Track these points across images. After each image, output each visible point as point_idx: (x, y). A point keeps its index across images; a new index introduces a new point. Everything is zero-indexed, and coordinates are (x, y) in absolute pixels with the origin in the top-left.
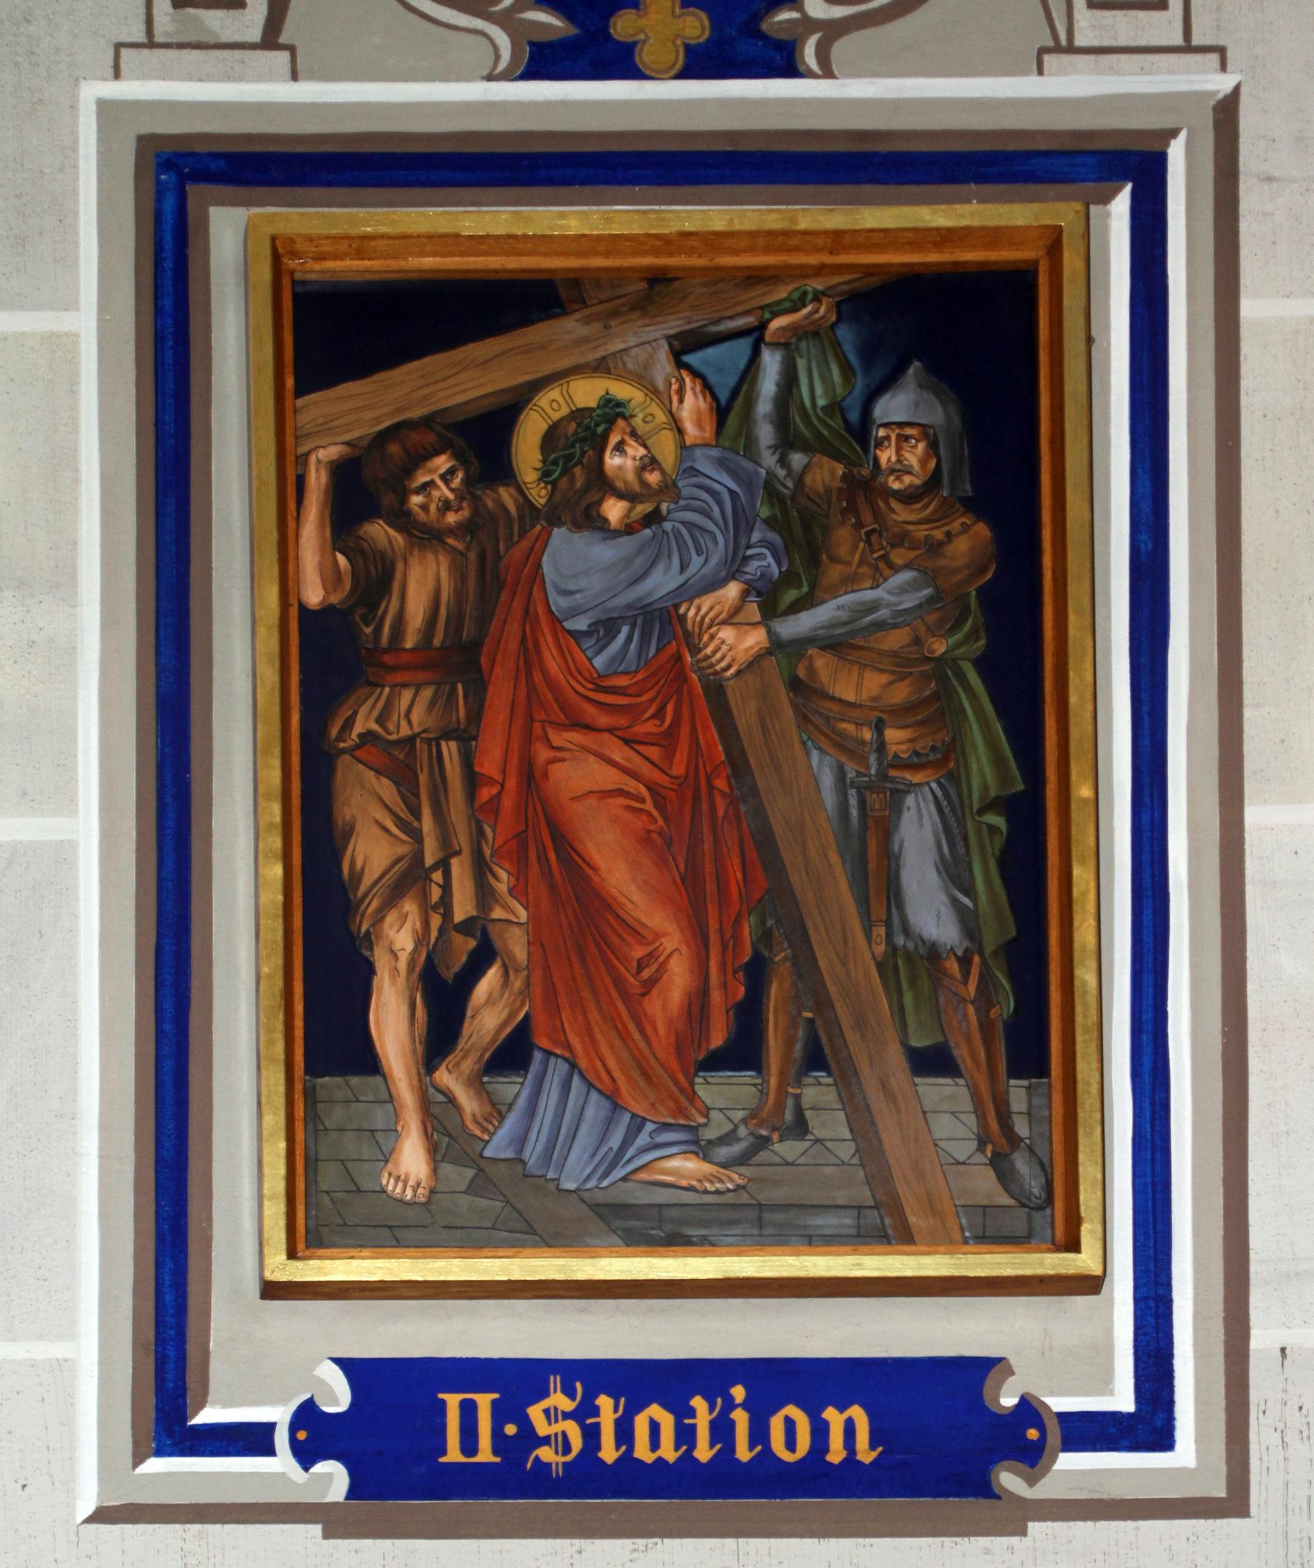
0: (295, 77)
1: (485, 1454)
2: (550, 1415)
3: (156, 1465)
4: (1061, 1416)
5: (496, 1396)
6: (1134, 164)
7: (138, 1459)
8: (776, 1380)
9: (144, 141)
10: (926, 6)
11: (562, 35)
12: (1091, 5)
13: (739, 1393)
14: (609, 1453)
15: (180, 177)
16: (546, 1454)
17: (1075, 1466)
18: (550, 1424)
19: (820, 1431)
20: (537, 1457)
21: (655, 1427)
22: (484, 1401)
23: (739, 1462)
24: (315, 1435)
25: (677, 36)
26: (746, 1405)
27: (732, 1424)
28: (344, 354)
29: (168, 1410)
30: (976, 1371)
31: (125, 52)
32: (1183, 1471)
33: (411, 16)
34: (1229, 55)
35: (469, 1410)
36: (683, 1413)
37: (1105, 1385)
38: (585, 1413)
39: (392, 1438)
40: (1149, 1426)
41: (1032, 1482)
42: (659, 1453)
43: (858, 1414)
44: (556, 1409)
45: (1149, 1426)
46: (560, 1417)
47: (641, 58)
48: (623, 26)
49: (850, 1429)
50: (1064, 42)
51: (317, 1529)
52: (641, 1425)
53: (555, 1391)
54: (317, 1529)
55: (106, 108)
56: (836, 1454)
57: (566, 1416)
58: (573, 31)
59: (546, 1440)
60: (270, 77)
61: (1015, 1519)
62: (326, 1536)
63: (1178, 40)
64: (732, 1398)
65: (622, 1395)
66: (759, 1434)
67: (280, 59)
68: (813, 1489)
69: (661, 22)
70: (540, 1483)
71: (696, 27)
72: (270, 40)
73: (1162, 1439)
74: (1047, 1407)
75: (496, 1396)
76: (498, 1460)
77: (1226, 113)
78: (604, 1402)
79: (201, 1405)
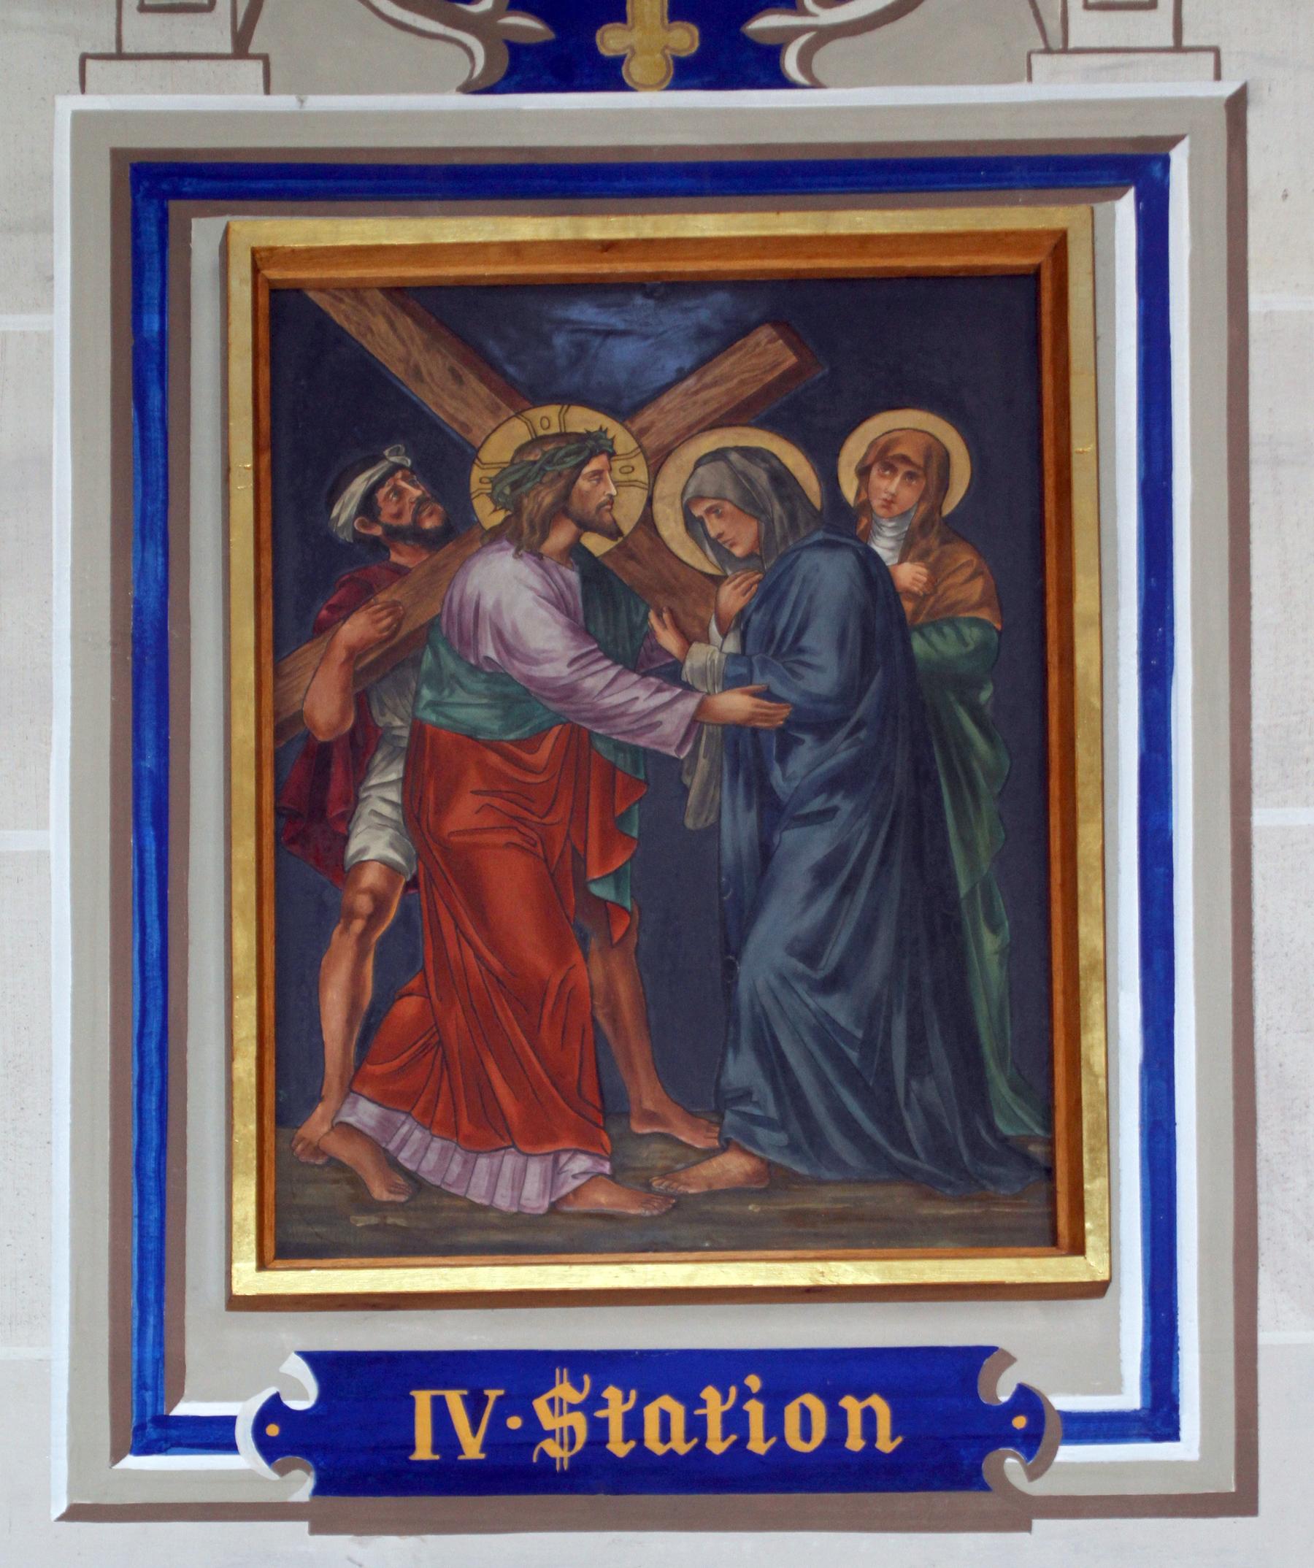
3: (133, 1462)
6: (1135, 168)
7: (117, 1456)
8: (787, 1373)
9: (117, 155)
10: (924, 4)
11: (540, 39)
14: (619, 1447)
15: (157, 191)
16: (552, 1448)
19: (837, 1418)
21: (665, 1418)
24: (282, 1434)
25: (666, 47)
30: (971, 1362)
36: (692, 1401)
37: (1115, 1387)
39: (356, 1438)
41: (1033, 1475)
42: (669, 1446)
44: (561, 1400)
45: (1159, 1418)
46: (565, 1406)
48: (610, 40)
49: (873, 1422)
50: (1056, 43)
51: (304, 1526)
52: (651, 1414)
53: (562, 1382)
54: (304, 1526)
55: (80, 119)
56: (855, 1442)
57: (572, 1408)
58: (551, 35)
59: (551, 1434)
61: (1019, 1515)
65: (632, 1387)
66: (774, 1425)
67: (253, 69)
69: (647, 31)
71: (686, 39)
72: (241, 49)
76: (437, 1457)
77: (1237, 106)
78: (612, 1394)
79: (178, 1396)
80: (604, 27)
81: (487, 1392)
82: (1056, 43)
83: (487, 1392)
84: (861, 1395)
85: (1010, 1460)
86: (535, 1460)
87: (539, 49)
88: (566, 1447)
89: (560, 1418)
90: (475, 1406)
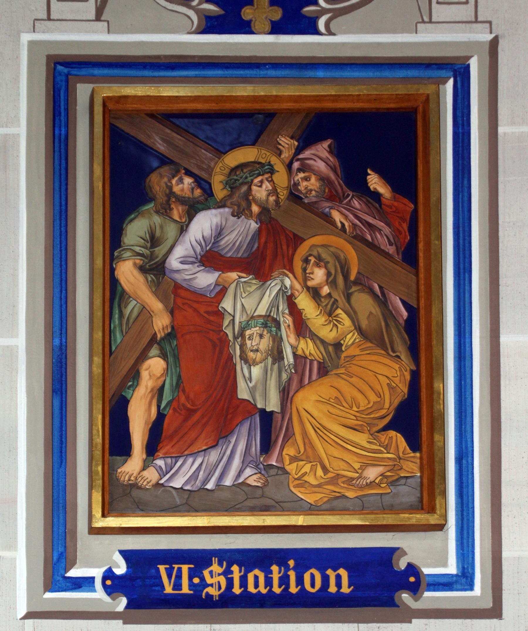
1: (185, 589)
2: (214, 579)
3: (48, 595)
5: (192, 566)
8: (306, 559)
9: (49, 58)
10: (373, 2)
11: (216, 14)
12: (438, 3)
13: (291, 563)
14: (237, 590)
15: (63, 73)
16: (210, 590)
19: (325, 579)
21: (256, 578)
22: (185, 568)
23: (292, 594)
24: (113, 584)
26: (294, 568)
27: (288, 577)
30: (388, 555)
31: (36, 21)
32: (476, 597)
36: (268, 573)
37: (445, 564)
38: (227, 572)
41: (416, 600)
43: (343, 572)
45: (464, 579)
47: (255, 29)
48: (247, 13)
49: (341, 581)
50: (426, 19)
51: (121, 621)
52: (251, 577)
54: (121, 621)
55: (32, 44)
56: (333, 589)
58: (222, 12)
59: (212, 585)
61: (409, 615)
64: (289, 565)
66: (300, 581)
68: (323, 603)
69: (261, 11)
70: (209, 603)
71: (277, 14)
72: (98, 18)
74: (422, 572)
75: (192, 566)
76: (192, 592)
77: (494, 45)
78: (235, 568)
81: (174, 566)
82: (426, 19)
83: (174, 566)
85: (404, 595)
87: (217, 18)
88: (217, 590)
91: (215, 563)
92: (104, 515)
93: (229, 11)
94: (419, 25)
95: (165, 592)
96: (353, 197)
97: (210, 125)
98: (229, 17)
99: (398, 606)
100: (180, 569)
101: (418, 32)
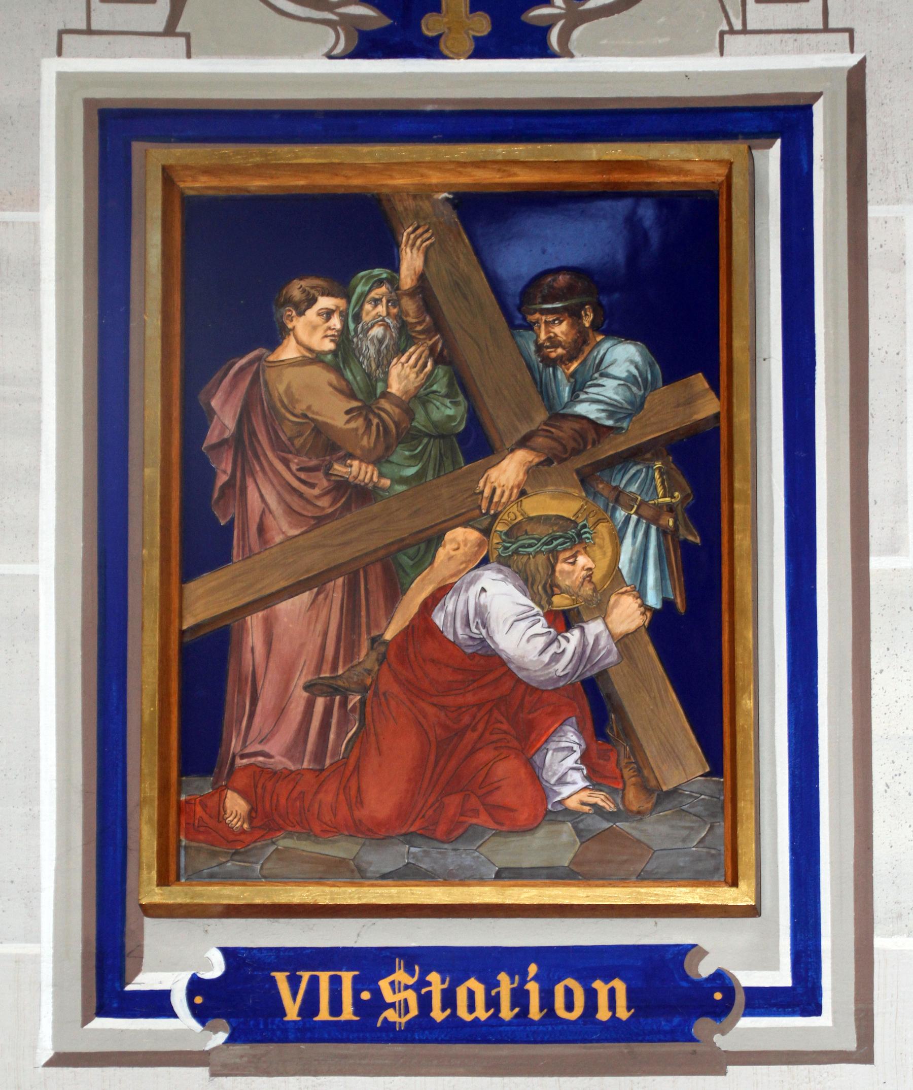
0: (189, 56)
1: (348, 1013)
2: (397, 990)
4: (749, 991)
5: (357, 973)
6: (785, 120)
7: (86, 1020)
8: (558, 962)
11: (375, 27)
13: (533, 969)
14: (438, 1014)
15: (119, 131)
16: (390, 1015)
17: (751, 1029)
18: (394, 993)
19: (591, 996)
20: (385, 1018)
21: (471, 994)
22: (347, 977)
24: (208, 999)
26: (536, 978)
28: (210, 236)
29: (109, 986)
30: (678, 954)
33: (284, 19)
34: (856, 35)
35: (336, 983)
36: (491, 984)
40: (802, 997)
43: (620, 986)
44: (400, 983)
45: (802, 997)
48: (430, 25)
50: (738, 26)
53: (400, 968)
55: (62, 78)
56: (603, 1014)
57: (407, 987)
58: (386, 22)
59: (392, 1005)
60: (173, 55)
61: (717, 1063)
62: (214, 1074)
63: (821, 26)
70: (390, 1034)
71: (482, 25)
72: (170, 30)
73: (815, 1009)
75: (357, 973)
77: (856, 78)
78: (434, 977)
80: (427, 16)
82: (738, 26)
84: (607, 979)
86: (379, 1025)
89: (397, 990)
90: (294, 983)
91: (400, 968)
92: (163, 880)
93: (399, 19)
94: (726, 37)
95: (286, 1019)
96: (635, 395)
97: (530, 462)
98: (399, 28)
99: (698, 1041)
100: (314, 981)
101: (855, 48)
